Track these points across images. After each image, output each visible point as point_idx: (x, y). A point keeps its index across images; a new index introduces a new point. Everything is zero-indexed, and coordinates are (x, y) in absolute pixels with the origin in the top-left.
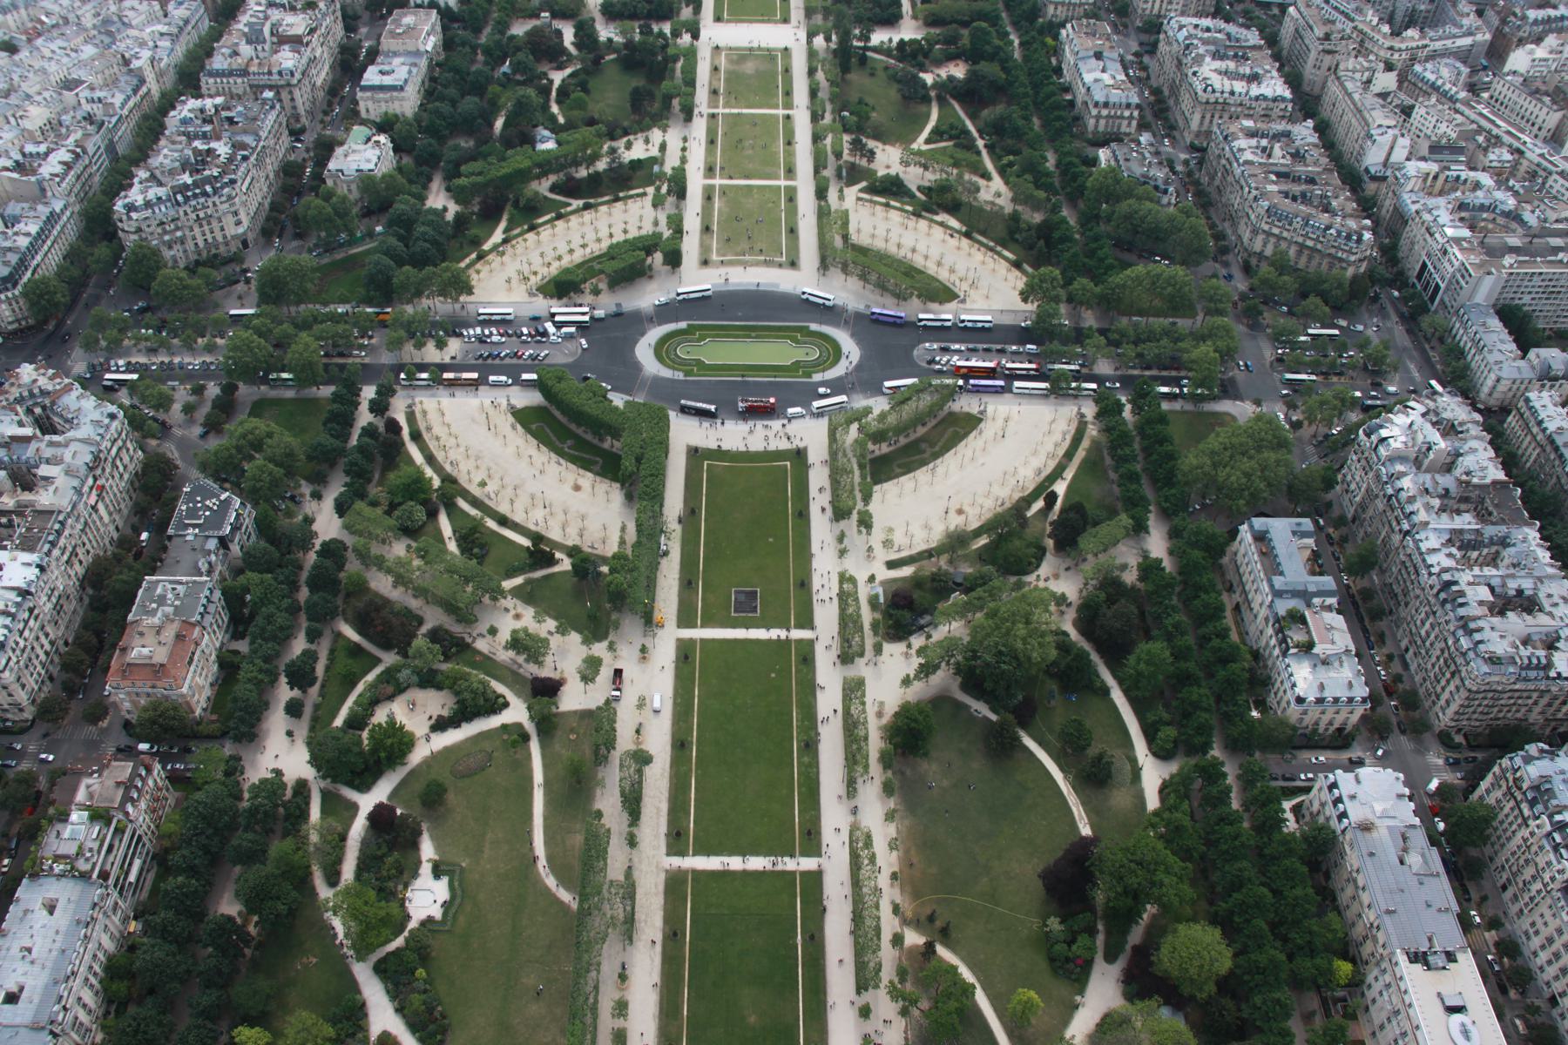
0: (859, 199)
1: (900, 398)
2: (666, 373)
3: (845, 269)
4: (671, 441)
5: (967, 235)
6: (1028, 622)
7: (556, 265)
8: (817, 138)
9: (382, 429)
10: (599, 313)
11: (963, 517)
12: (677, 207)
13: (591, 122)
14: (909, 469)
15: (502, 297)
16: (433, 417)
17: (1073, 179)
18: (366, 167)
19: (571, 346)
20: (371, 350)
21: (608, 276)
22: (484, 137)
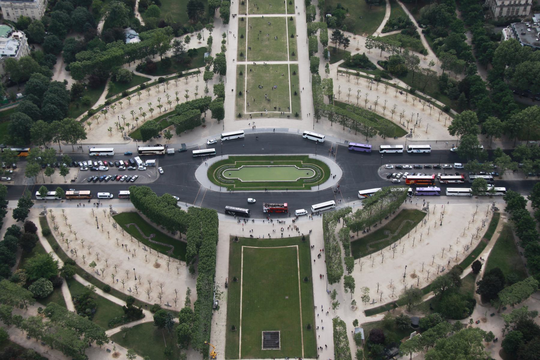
0: (339, 71)
1: (370, 201)
2: (215, 188)
3: (331, 118)
4: (220, 233)
5: (412, 92)
6: (466, 353)
7: (141, 119)
8: (310, 32)
9: (22, 229)
10: (171, 150)
11: (416, 280)
12: (221, 80)
13: (162, 25)
14: (377, 248)
15: (106, 140)
16: (59, 220)
17: (485, 51)
18: (9, 53)
19: (152, 172)
20: (15, 176)
21: (176, 125)
22: (90, 33)
